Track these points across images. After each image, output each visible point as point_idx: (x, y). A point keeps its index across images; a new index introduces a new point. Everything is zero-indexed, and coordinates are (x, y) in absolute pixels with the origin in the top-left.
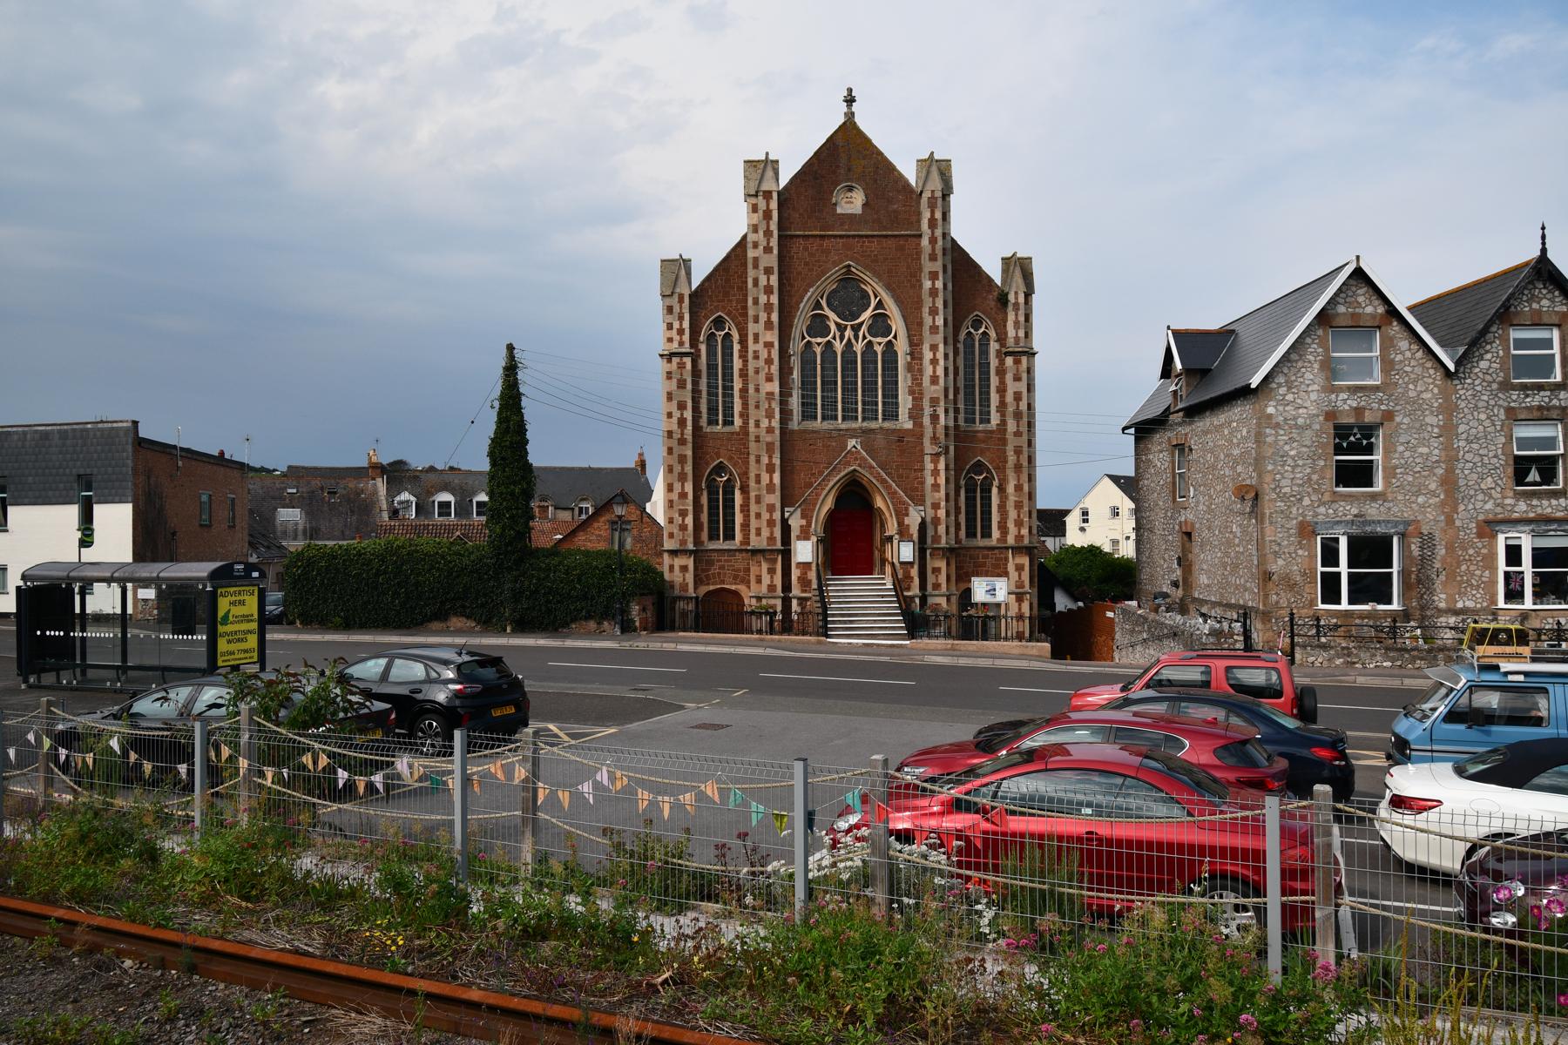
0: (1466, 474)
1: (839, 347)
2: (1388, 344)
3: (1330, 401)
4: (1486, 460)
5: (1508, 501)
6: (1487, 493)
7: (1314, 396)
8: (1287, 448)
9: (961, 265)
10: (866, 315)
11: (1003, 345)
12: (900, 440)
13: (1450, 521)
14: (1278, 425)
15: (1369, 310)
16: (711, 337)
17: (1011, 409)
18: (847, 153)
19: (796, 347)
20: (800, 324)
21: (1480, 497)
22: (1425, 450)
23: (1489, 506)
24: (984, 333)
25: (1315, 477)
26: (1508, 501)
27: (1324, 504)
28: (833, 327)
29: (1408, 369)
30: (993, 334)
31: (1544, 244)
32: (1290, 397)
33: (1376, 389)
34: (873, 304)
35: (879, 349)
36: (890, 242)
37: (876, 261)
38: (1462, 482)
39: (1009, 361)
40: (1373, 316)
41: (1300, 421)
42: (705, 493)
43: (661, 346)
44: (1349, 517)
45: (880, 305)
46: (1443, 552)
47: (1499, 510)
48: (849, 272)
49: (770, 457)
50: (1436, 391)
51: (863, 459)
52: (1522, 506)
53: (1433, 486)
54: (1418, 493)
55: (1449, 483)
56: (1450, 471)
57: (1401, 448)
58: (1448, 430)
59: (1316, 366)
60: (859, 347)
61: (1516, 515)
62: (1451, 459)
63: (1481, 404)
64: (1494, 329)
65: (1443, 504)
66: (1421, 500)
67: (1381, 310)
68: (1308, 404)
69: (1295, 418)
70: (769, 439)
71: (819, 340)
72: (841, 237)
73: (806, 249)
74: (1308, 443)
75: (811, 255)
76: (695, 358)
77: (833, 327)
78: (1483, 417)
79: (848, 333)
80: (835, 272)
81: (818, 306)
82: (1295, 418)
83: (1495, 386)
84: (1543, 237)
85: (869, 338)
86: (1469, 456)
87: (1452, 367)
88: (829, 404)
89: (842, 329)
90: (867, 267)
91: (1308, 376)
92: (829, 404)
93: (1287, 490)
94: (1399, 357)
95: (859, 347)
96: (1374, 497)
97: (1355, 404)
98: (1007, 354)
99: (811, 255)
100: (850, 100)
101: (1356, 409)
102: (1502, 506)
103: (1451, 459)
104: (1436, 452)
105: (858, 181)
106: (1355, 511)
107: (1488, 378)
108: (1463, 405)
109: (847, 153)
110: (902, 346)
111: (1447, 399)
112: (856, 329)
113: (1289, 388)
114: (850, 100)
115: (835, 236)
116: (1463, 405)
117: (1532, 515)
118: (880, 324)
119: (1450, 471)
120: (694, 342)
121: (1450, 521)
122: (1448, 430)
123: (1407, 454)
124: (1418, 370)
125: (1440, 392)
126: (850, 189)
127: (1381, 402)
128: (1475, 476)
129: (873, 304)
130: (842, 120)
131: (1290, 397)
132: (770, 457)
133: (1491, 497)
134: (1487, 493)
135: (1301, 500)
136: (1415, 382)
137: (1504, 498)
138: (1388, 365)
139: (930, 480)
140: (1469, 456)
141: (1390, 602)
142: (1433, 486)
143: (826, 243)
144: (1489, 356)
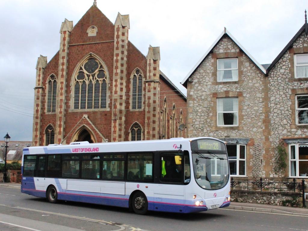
0: (274, 119)
1: (87, 82)
2: (241, 64)
3: (215, 88)
4: (283, 112)
5: (293, 130)
6: (284, 126)
7: (209, 87)
8: (198, 108)
9: (132, 51)
10: (96, 71)
11: (146, 79)
12: (106, 115)
13: (267, 139)
14: (194, 100)
15: (233, 51)
16: (50, 81)
17: (146, 103)
18: (94, 16)
19: (73, 83)
20: (75, 75)
21: (281, 128)
22: (256, 108)
23: (285, 132)
24: (140, 75)
25: (208, 120)
26: (293, 130)
27: (212, 131)
28: (86, 76)
29: (249, 74)
30: (142, 75)
31: (306, 18)
32: (199, 88)
33: (235, 83)
34: (99, 66)
35: (80, 84)
36: (104, 45)
37: (100, 52)
38: (272, 122)
39: (147, 84)
40: (234, 53)
41: (203, 97)
42: (45, 136)
43: (35, 86)
44: (224, 137)
45: (101, 66)
46: (264, 152)
47: (289, 134)
48: (91, 56)
49: (60, 122)
50: (261, 83)
51: (87, 121)
52: (299, 132)
53: (260, 124)
54: (253, 127)
55: (267, 122)
56: (267, 116)
57: (246, 108)
58: (266, 99)
59: (211, 74)
60: (94, 82)
61: (296, 136)
62: (267, 112)
63: (281, 88)
64: (287, 55)
65: (264, 131)
66: (255, 129)
67: (238, 50)
68: (206, 90)
69: (201, 96)
70: (60, 115)
71: (81, 80)
72: (89, 44)
73: (77, 49)
74: (206, 106)
75: (79, 51)
76: (43, 89)
77: (86, 76)
78: (281, 93)
79: (91, 77)
80: (87, 57)
81: (81, 68)
82: (201, 96)
83: (287, 80)
84: (306, 16)
85: (97, 79)
86: (275, 111)
87: (265, 72)
88: (83, 103)
89: (88, 76)
90: (97, 54)
91: (207, 79)
92: (83, 103)
93: (197, 126)
94: (245, 69)
95: (94, 82)
96: (232, 128)
97: (225, 89)
98: (147, 82)
99: (79, 51)
100: (306, 12)
101: (226, 91)
102: (290, 132)
103: (267, 112)
104: (261, 109)
105: (96, 25)
106: (226, 135)
107: (284, 77)
108: (273, 88)
109: (94, 16)
110: (107, 81)
111: (266, 86)
112: (93, 76)
113: (200, 84)
114: (306, 12)
115: (87, 44)
116: (273, 88)
117: (304, 136)
118: (101, 74)
119: (267, 116)
120: (44, 83)
121: (267, 139)
122: (266, 99)
123: (248, 110)
124: (253, 74)
125: (263, 83)
126: (93, 28)
127: (237, 88)
128: (278, 119)
129: (99, 66)
130: (92, 4)
131: (199, 88)
132: (60, 122)
133: (285, 128)
134: (284, 126)
135: (203, 130)
136: (252, 79)
137: (291, 128)
138: (241, 73)
139: (113, 129)
140: (275, 111)
141: (236, 174)
142: (260, 124)
143: (84, 47)
144: (284, 67)
